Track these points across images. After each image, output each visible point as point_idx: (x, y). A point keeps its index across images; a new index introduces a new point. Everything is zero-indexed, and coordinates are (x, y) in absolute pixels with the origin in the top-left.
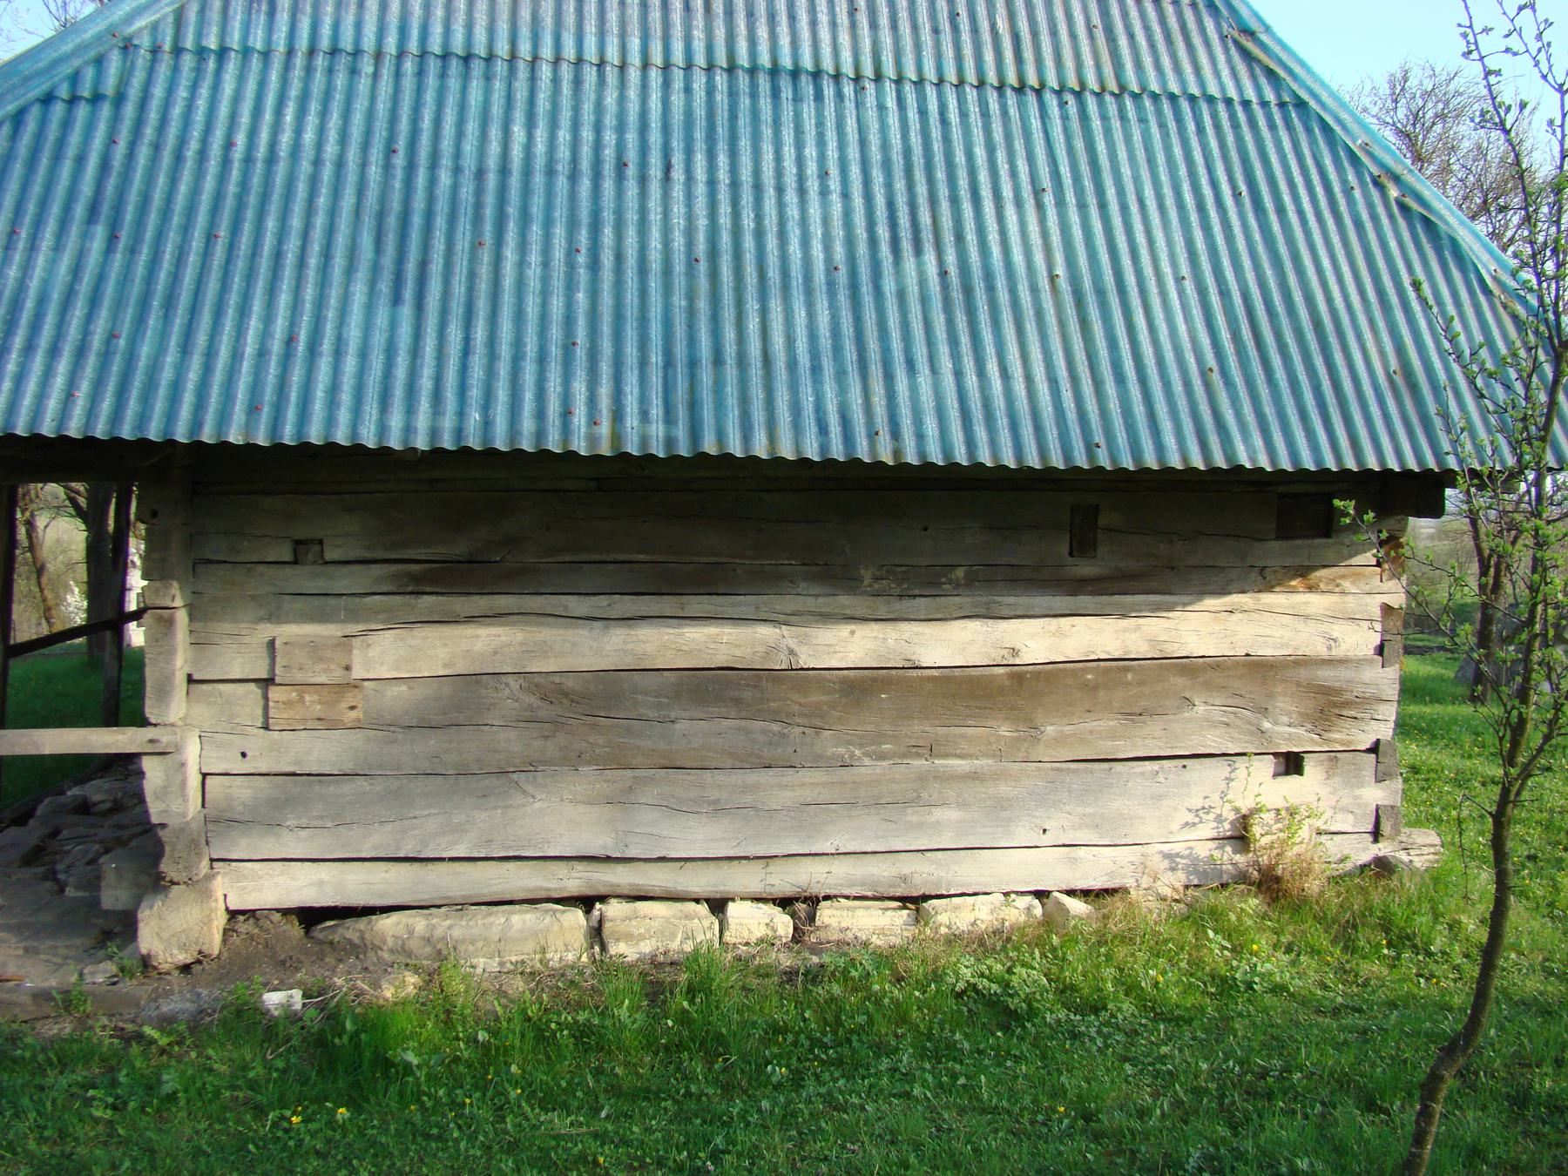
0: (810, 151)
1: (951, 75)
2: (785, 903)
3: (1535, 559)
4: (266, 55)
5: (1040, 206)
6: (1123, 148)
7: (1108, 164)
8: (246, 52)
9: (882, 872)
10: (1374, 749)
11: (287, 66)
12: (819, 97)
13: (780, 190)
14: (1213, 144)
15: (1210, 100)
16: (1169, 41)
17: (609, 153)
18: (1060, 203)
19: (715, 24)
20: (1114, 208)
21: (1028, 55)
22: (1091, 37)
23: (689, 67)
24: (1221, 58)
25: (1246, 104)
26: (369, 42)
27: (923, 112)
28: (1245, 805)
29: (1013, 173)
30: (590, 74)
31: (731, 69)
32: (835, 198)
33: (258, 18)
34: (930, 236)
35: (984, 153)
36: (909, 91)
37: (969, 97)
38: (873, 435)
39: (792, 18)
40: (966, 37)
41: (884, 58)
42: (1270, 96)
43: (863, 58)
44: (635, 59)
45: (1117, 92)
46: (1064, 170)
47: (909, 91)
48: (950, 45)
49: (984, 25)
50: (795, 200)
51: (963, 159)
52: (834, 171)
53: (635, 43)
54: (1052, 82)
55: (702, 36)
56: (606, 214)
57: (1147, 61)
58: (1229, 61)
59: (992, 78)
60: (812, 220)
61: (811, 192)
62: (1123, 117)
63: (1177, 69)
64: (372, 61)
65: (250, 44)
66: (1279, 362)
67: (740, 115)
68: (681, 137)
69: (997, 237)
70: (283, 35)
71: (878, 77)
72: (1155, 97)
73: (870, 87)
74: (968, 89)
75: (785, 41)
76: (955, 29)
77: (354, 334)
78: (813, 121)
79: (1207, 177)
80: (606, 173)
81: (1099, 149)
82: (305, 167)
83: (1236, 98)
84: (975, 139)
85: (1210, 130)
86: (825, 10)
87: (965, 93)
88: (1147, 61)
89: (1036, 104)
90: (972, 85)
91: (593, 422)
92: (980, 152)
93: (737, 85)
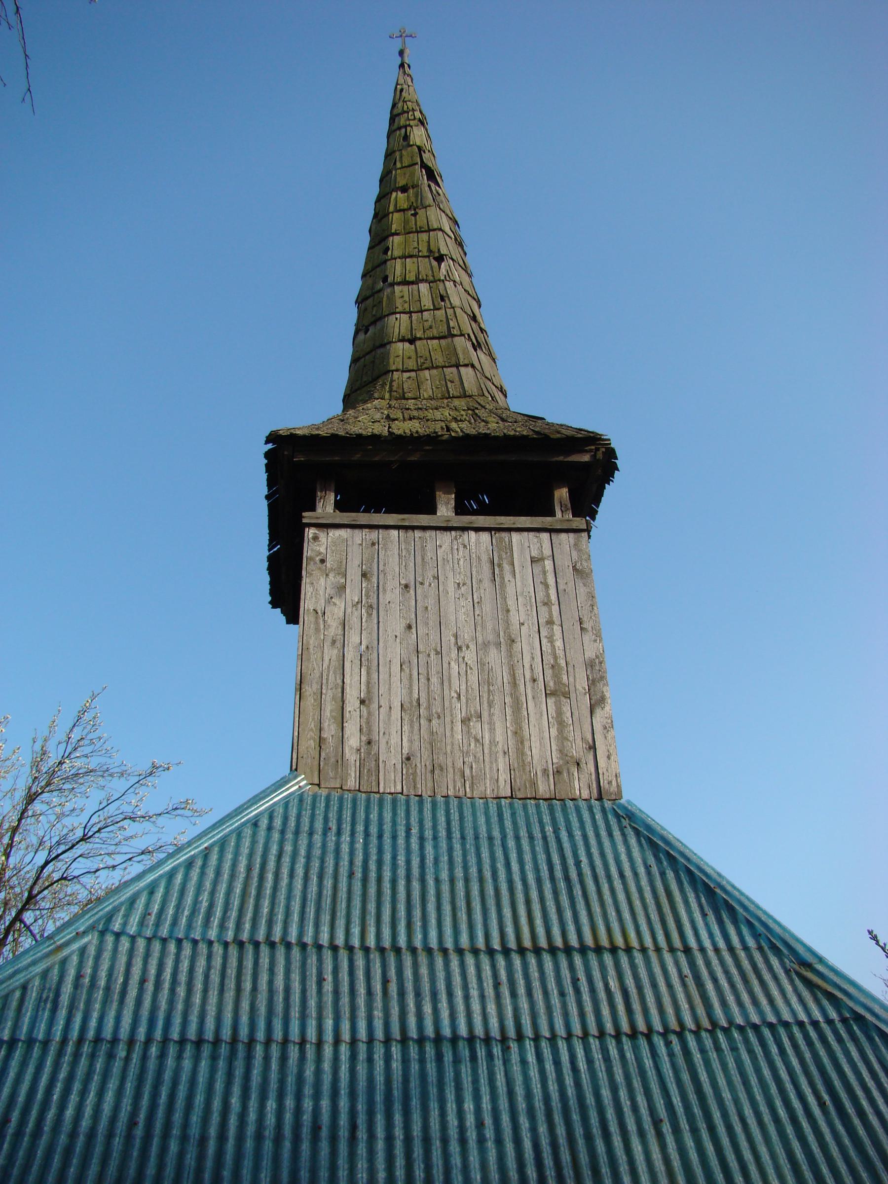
1: (577, 1030)
3: (345, 576)
4: (46, 1043)
5: (660, 1135)
6: (722, 1075)
8: (30, 1042)
11: (60, 1053)
12: (474, 1058)
14: (795, 1062)
15: (786, 1025)
18: (676, 1130)
19: (391, 1004)
21: (636, 1006)
22: (684, 985)
24: (788, 988)
25: (815, 1024)
26: (124, 1033)
27: (557, 1063)
29: (635, 1108)
30: (294, 1052)
31: (404, 1040)
32: (490, 1145)
33: (43, 1014)
34: (571, 1172)
35: (609, 1093)
37: (593, 1047)
40: (586, 997)
41: (523, 1021)
42: (833, 1015)
43: (507, 1023)
44: (329, 1037)
45: (710, 1028)
46: (676, 1100)
48: (574, 1005)
49: (600, 986)
50: (458, 1149)
51: (593, 1100)
53: (329, 1023)
54: (658, 1026)
55: (381, 1015)
56: (302, 1172)
57: (730, 999)
59: (609, 1027)
60: (472, 1166)
61: (471, 1142)
62: (718, 1048)
63: (755, 1002)
64: (126, 1047)
65: (34, 1036)
66: (719, 1080)
67: (412, 1079)
68: (365, 1101)
69: (627, 1167)
70: (60, 1028)
71: (520, 1037)
72: (741, 1029)
73: (514, 1046)
74: (591, 1040)
75: (445, 1014)
76: (577, 991)
78: (470, 1079)
79: (794, 1091)
80: (304, 1136)
81: (702, 1079)
83: (806, 1020)
84: (601, 1083)
85: (790, 1051)
86: (475, 986)
87: (589, 1044)
88: (730, 999)
89: (647, 1047)
90: (594, 1036)
93: (409, 1054)
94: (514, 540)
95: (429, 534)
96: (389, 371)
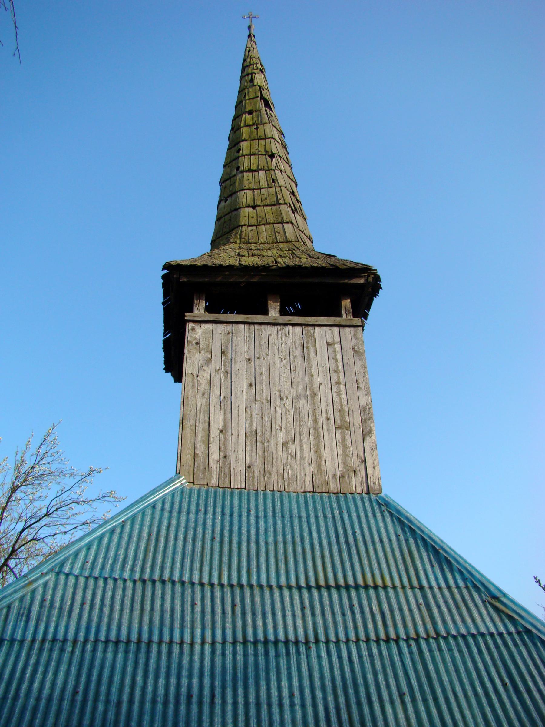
0: (285, 683)
1: (352, 637)
4: (22, 642)
5: (403, 703)
6: (442, 666)
7: (435, 676)
11: (31, 648)
12: (288, 654)
13: (269, 705)
14: (488, 658)
15: (483, 635)
17: (184, 690)
18: (414, 700)
20: (442, 700)
21: (390, 623)
22: (419, 609)
23: (224, 642)
24: (484, 612)
25: (501, 635)
26: (71, 636)
27: (340, 657)
29: (388, 686)
30: (176, 649)
31: (245, 642)
32: (298, 708)
33: (21, 623)
36: (332, 646)
37: (362, 647)
39: (274, 614)
41: (319, 631)
42: (512, 629)
44: (198, 639)
45: (435, 637)
47: (332, 646)
49: (367, 609)
50: (277, 710)
51: (362, 680)
52: (297, 693)
53: (198, 631)
54: (403, 635)
56: (181, 724)
57: (448, 618)
58: (489, 613)
59: (372, 636)
60: (286, 721)
61: (285, 706)
62: (440, 649)
64: (72, 645)
65: (15, 637)
68: (220, 679)
69: (382, 723)
70: (31, 632)
71: (317, 641)
72: (454, 637)
73: (313, 646)
74: (361, 643)
76: (353, 613)
78: (285, 667)
81: (430, 668)
82: (32, 701)
84: (367, 670)
86: (290, 609)
87: (360, 645)
88: (448, 618)
89: (396, 648)
90: (363, 641)
92: (370, 676)
93: (247, 651)
94: (316, 332)
95: (263, 327)
96: (239, 226)
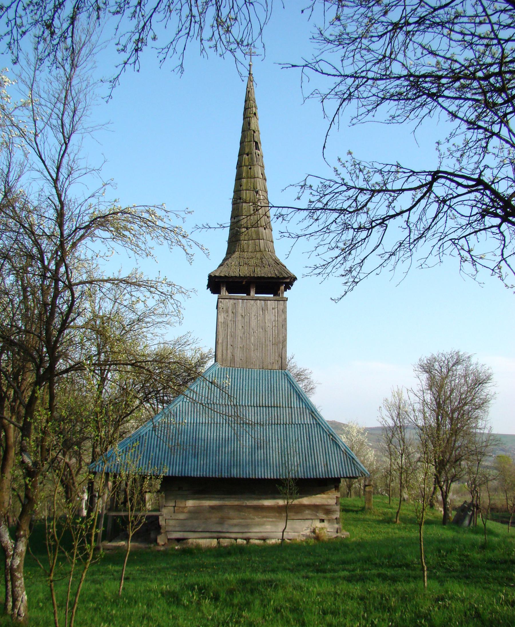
2: (245, 539)
9: (260, 535)
10: (336, 519)
16: (300, 414)
24: (308, 416)
28: (314, 527)
30: (218, 425)
38: (252, 475)
77: (190, 462)
91: (219, 473)
92: (270, 434)
